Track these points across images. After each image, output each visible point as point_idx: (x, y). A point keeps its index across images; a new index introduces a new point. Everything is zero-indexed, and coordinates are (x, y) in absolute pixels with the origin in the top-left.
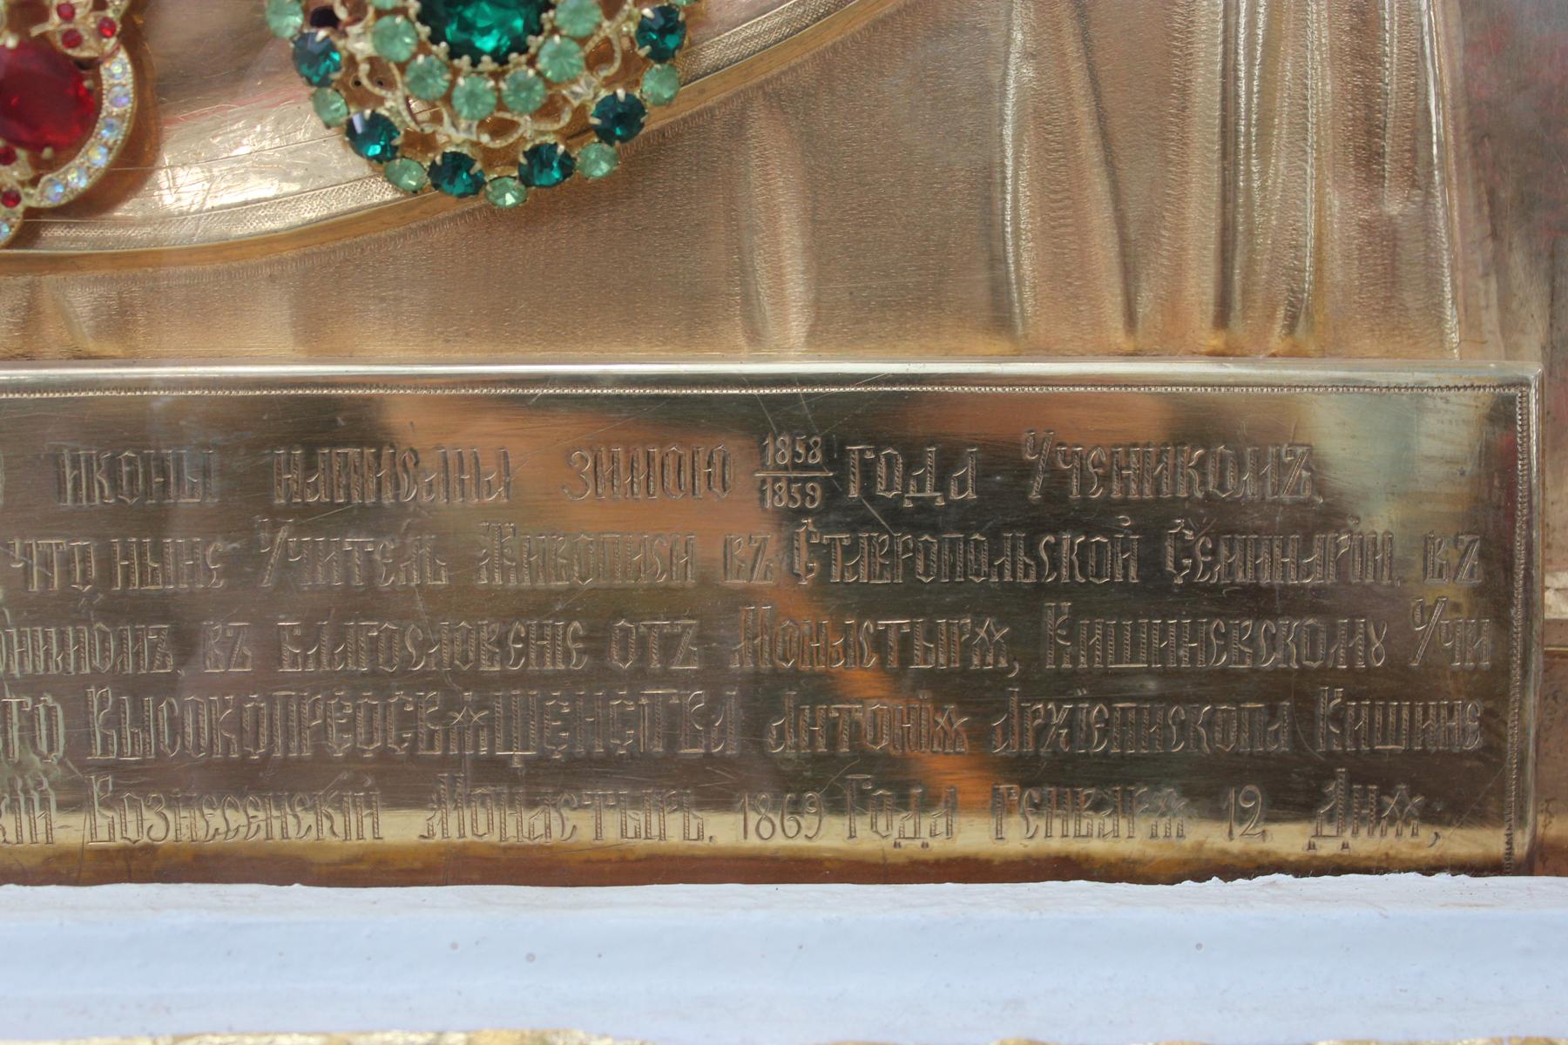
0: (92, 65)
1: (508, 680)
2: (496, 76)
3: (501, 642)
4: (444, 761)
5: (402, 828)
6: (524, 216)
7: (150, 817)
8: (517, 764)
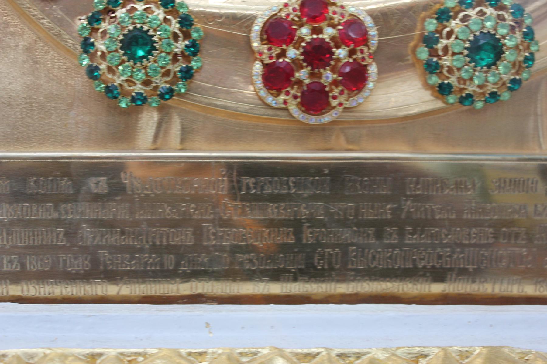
0: (366, 66)
1: (470, 245)
3: (469, 234)
7: (31, 288)
8: (471, 270)
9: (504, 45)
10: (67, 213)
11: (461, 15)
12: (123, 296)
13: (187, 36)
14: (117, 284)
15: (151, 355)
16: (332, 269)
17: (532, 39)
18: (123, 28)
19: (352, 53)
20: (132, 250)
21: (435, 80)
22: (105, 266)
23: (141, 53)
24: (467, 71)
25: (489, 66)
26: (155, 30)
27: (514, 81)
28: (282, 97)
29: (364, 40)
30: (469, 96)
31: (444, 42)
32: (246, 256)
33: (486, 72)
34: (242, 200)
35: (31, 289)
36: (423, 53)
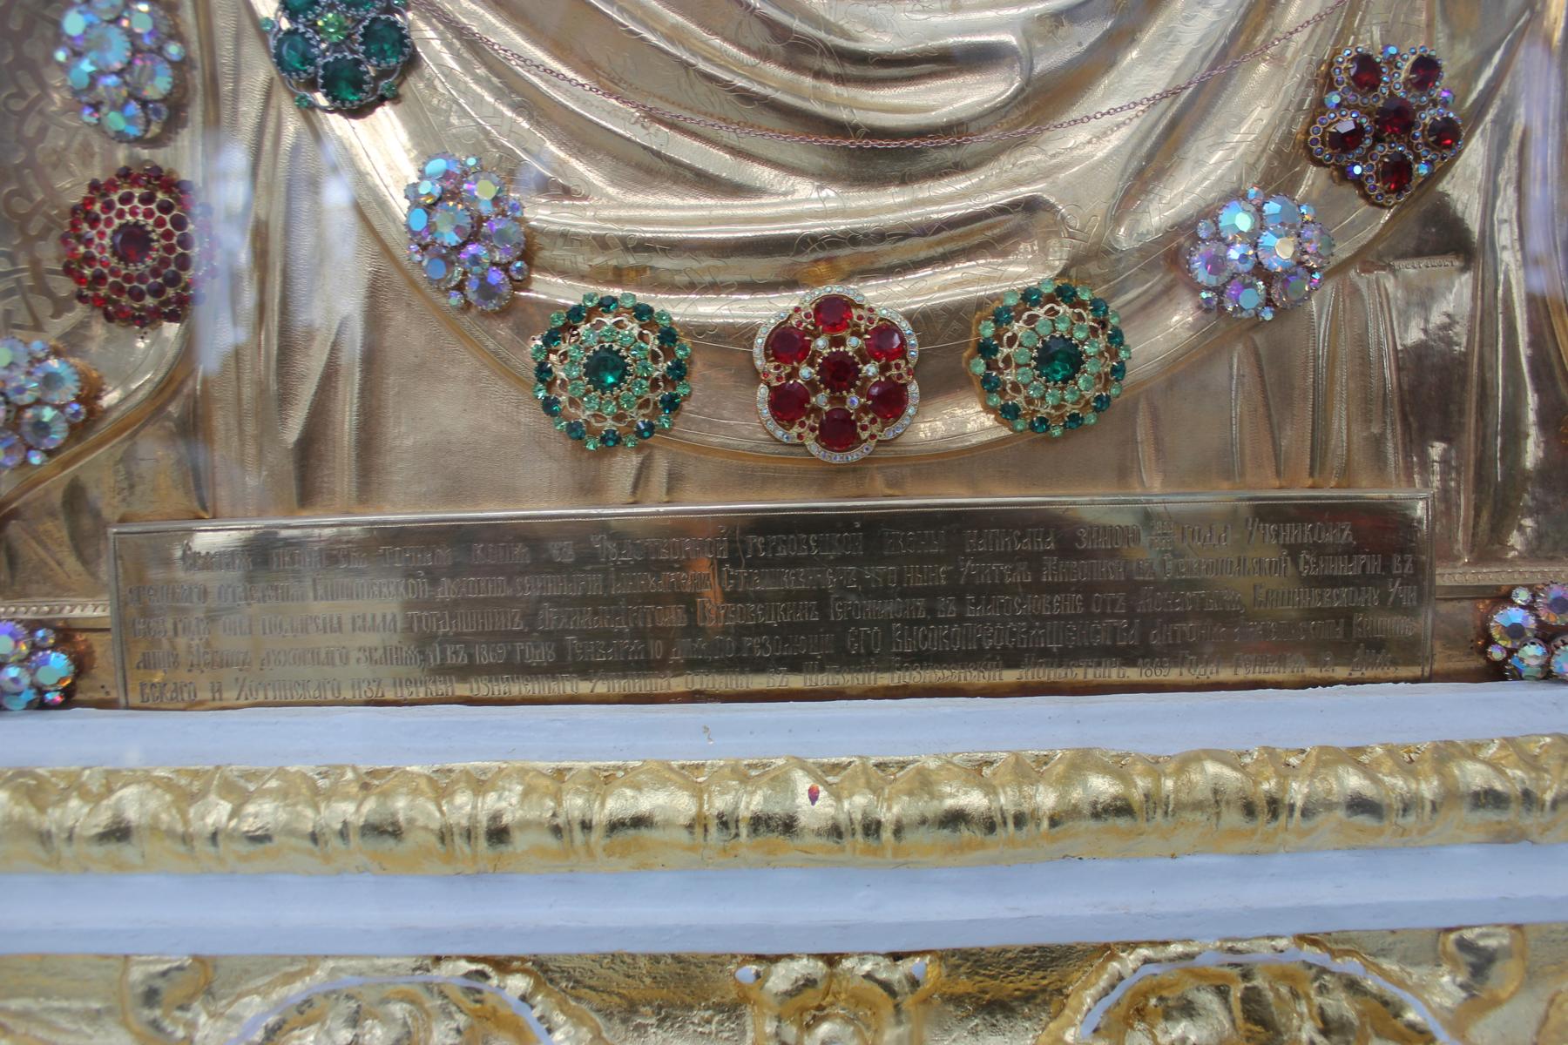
0: (905, 386)
1: (1053, 617)
2: (1062, 389)
3: (1051, 603)
4: (1027, 650)
5: (1010, 676)
6: (1064, 437)
9: (1081, 353)
10: (523, 589)
11: (1025, 316)
12: (599, 695)
13: (669, 354)
14: (590, 680)
15: (633, 769)
16: (870, 654)
17: (1121, 343)
18: (587, 349)
19: (884, 369)
20: (607, 635)
21: (995, 400)
22: (574, 655)
23: (610, 380)
24: (1035, 388)
25: (1065, 380)
26: (628, 349)
27: (1099, 398)
28: (796, 430)
29: (902, 352)
30: (1043, 421)
31: (1006, 350)
32: (757, 640)
33: (1062, 389)
34: (748, 566)
35: (482, 688)
36: (979, 367)
